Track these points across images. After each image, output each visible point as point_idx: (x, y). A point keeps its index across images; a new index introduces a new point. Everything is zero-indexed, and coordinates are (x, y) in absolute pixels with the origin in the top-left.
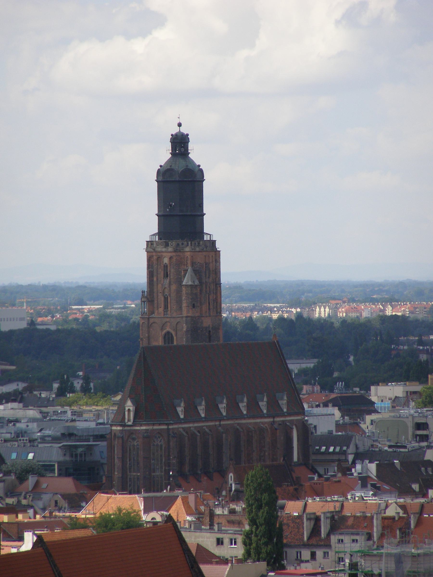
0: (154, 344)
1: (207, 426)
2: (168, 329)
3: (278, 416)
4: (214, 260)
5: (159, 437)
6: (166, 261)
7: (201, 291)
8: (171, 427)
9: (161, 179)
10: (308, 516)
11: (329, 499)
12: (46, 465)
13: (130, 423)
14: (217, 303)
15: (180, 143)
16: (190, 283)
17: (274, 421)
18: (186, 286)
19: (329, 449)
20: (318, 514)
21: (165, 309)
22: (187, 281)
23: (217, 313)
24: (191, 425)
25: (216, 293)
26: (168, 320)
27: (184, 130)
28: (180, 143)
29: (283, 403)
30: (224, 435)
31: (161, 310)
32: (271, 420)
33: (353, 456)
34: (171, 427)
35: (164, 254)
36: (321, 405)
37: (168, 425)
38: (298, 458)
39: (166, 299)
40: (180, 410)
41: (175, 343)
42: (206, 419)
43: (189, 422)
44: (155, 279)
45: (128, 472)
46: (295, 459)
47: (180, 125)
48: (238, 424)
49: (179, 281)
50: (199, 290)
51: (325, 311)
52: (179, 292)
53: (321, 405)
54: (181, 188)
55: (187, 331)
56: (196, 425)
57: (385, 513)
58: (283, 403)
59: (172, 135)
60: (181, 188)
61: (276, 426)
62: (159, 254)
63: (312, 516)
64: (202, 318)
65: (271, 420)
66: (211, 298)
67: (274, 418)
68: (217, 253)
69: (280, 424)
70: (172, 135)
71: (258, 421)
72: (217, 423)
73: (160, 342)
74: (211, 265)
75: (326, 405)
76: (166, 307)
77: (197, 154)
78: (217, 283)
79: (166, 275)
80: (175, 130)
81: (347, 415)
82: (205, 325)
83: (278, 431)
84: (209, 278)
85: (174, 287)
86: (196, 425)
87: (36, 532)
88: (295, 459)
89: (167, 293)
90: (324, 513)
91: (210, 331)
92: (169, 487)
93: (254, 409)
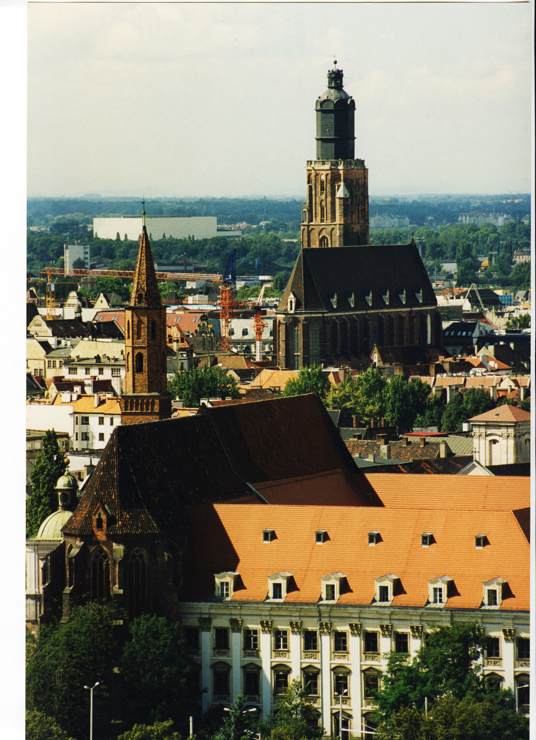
0: (313, 246)
1: (355, 315)
2: (324, 234)
3: (415, 306)
4: (363, 176)
5: (316, 324)
6: (323, 177)
7: (352, 202)
8: (325, 315)
9: (319, 108)
10: (437, 389)
11: (454, 375)
12: (304, 342)
13: (292, 312)
14: (365, 212)
15: (336, 78)
16: (342, 196)
17: (411, 310)
18: (340, 198)
19: (457, 333)
20: (444, 387)
21: (321, 217)
22: (341, 193)
23: (365, 221)
24: (342, 314)
25: (364, 205)
26: (324, 227)
27: (339, 67)
28: (336, 78)
29: (420, 296)
30: (370, 322)
31: (319, 218)
32: (410, 309)
33: (477, 339)
34: (325, 315)
35: (321, 172)
36: (455, 297)
37: (323, 313)
38: (431, 341)
39: (322, 209)
40: (334, 300)
41: (330, 246)
42: (372, 308)
43: (376, 309)
44: (314, 192)
45: (145, 358)
46: (429, 342)
47: (335, 62)
48: (382, 313)
49: (333, 194)
50: (350, 201)
51: (466, 219)
52: (333, 203)
53: (455, 297)
54: (338, 119)
55: (340, 236)
56: (346, 313)
57: (500, 386)
58: (420, 296)
59: (342, 71)
60: (338, 119)
61: (413, 315)
62: (317, 172)
63: (440, 388)
64: (353, 225)
65: (410, 309)
66: (360, 208)
67: (411, 308)
68: (365, 170)
69: (416, 313)
70: (342, 71)
71: (399, 310)
72: (365, 312)
73: (315, 245)
74: (360, 181)
75: (458, 297)
76: (322, 216)
77: (348, 87)
78: (366, 196)
79: (322, 189)
80: (333, 68)
81: (475, 305)
82: (355, 231)
83: (415, 319)
84: (358, 191)
85: (329, 199)
86: (346, 313)
87: (210, 400)
88: (429, 342)
89: (324, 203)
90: (450, 386)
91: (359, 236)
92: (323, 364)
93: (395, 302)
